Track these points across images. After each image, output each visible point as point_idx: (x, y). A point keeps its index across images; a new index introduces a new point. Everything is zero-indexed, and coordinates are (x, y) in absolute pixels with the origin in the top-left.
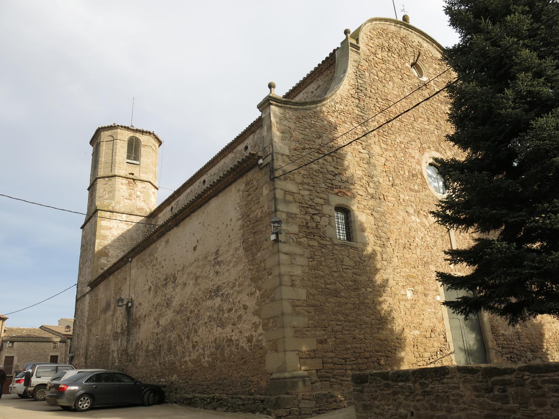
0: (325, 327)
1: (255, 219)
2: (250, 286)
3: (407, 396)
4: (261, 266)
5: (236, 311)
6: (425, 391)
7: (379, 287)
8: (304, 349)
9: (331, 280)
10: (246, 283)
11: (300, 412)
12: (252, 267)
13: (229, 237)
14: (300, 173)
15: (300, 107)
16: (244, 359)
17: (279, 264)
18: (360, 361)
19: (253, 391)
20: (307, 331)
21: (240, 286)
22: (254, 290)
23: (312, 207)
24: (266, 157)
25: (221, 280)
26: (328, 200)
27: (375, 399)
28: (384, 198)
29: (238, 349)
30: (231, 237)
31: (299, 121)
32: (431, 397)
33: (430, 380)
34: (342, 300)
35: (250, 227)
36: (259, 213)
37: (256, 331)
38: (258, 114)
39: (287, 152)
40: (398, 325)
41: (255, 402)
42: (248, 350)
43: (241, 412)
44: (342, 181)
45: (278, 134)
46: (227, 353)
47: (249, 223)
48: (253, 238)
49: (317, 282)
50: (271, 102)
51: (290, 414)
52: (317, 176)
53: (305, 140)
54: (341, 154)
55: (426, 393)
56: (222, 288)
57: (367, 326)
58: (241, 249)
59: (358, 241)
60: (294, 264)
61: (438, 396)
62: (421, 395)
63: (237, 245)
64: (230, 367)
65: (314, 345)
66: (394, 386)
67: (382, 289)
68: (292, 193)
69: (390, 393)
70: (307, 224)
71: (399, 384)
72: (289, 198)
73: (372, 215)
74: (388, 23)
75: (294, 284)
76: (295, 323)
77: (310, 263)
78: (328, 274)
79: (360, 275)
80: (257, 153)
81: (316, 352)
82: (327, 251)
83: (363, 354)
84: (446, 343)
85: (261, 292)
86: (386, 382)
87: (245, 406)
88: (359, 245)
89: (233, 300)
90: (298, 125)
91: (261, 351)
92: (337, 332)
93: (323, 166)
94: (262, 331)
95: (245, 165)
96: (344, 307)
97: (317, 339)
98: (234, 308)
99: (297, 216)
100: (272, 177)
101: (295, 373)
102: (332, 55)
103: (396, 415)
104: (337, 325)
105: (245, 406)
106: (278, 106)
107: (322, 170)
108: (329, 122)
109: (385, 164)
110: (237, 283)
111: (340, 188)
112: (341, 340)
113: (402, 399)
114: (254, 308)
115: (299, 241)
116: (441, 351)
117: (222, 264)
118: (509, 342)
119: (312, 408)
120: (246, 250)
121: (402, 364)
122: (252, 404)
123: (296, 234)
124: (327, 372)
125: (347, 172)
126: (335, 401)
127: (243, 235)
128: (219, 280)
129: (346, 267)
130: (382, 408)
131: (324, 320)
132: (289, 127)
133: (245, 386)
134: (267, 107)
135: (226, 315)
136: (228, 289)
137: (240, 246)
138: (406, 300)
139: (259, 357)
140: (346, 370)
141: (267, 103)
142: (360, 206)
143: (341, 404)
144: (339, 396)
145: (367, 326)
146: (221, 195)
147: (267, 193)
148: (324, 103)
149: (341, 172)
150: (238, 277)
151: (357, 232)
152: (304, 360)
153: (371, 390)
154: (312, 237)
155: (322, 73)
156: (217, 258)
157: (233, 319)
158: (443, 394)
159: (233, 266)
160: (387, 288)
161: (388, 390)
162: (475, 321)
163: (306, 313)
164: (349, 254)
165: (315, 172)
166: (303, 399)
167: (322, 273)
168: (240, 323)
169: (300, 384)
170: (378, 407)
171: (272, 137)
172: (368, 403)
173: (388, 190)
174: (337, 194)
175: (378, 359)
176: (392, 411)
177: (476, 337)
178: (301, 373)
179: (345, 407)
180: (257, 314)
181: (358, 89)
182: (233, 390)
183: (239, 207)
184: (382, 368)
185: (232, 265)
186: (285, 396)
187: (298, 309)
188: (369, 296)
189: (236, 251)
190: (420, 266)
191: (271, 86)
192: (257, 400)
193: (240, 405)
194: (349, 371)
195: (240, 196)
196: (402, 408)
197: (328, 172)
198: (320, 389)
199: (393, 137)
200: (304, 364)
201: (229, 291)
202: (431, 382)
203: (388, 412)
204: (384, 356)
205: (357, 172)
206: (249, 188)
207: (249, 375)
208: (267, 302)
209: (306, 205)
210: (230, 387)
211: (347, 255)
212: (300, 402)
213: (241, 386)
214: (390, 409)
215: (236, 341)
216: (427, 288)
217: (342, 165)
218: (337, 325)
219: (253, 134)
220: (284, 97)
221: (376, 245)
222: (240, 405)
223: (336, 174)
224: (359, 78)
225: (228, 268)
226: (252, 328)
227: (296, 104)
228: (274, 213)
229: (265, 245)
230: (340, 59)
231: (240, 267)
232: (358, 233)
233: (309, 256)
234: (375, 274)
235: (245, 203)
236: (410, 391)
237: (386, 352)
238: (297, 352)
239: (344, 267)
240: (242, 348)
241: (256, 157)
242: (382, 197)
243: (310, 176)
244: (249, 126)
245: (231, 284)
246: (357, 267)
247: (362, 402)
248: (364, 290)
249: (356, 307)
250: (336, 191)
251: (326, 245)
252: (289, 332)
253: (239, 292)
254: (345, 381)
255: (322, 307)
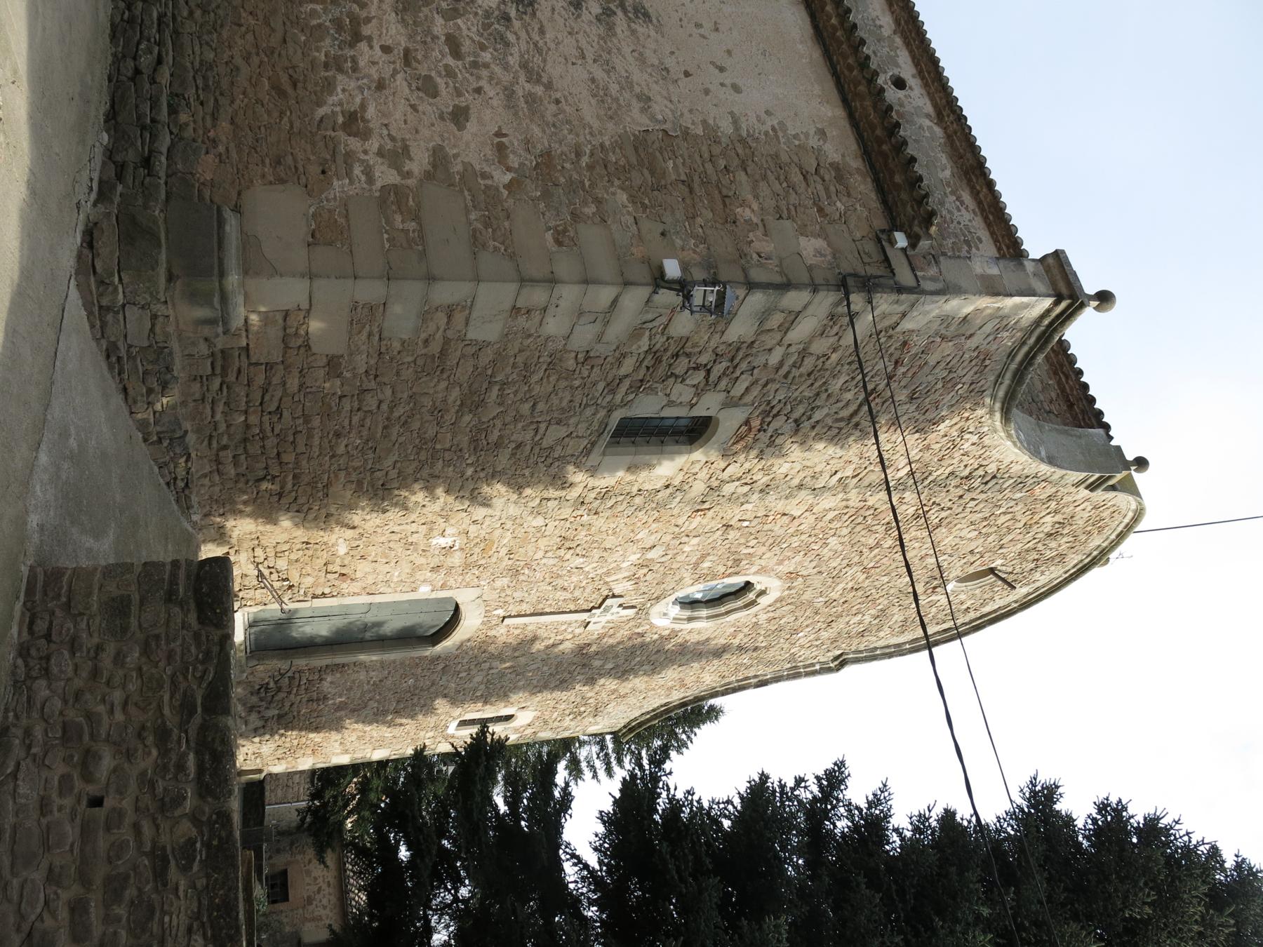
0: (376, 376)
1: (731, 194)
2: (528, 143)
3: (152, 784)
4: (585, 203)
5: (450, 73)
6: (165, 861)
7: (473, 490)
8: (315, 325)
9: (512, 396)
10: (537, 131)
11: (108, 309)
12: (585, 160)
13: (687, 74)
14: (834, 350)
15: (1013, 366)
16: (290, 90)
17: (586, 282)
18: (271, 442)
19: (183, 117)
20: (370, 335)
21: (531, 99)
22: (514, 161)
23: (731, 369)
24: (910, 264)
25: (552, 20)
26: (736, 405)
27: (146, 651)
28: (702, 510)
29: (326, 66)
30: (684, 82)
31: (977, 357)
32: (148, 883)
33: (201, 883)
34: (450, 417)
35: (709, 166)
36: (748, 213)
37: (380, 153)
38: (1036, 246)
39: (907, 325)
40: (366, 519)
41: (143, 128)
42: (321, 112)
43: (110, 58)
44: (777, 433)
45: (968, 309)
46: (313, 12)
47: (722, 163)
48: (674, 177)
49: (514, 366)
50: (1063, 305)
51: (101, 283)
52: (812, 384)
53: (920, 367)
54: (847, 438)
55: (160, 860)
56: (527, 18)
57: (370, 462)
58: (644, 122)
59: (606, 458)
60: (579, 317)
61: (152, 911)
62: (154, 843)
63: (660, 108)
64: (267, 22)
65: (322, 349)
66: (186, 732)
67: (467, 495)
68: (785, 328)
69: (162, 715)
70: (688, 355)
71: (191, 756)
72: (776, 320)
73: (667, 487)
74: (1113, 537)
75: (516, 313)
76: (396, 309)
77: (573, 355)
78: (530, 390)
79: (513, 455)
80: (929, 237)
81: (302, 350)
82: (597, 395)
83: (291, 449)
84: (310, 595)
85: (505, 193)
86: (199, 701)
87: (132, 79)
88: (594, 458)
89: (486, 66)
90: (966, 356)
91: (314, 170)
92: (360, 401)
93: (832, 400)
94: (379, 184)
95: (898, 179)
96: (428, 417)
97: (342, 356)
98: (460, 63)
99: (718, 336)
100: (850, 281)
101: (240, 299)
102: (1095, 419)
103: (92, 736)
104: (381, 402)
105: (132, 79)
106: (1043, 317)
107: (824, 396)
108: (943, 419)
109: (785, 514)
110: (539, 90)
111: (759, 431)
112: (335, 409)
113: (143, 765)
114: (456, 156)
115: (643, 334)
116: (291, 587)
117: (602, 31)
118: (303, 687)
119: (126, 336)
120: (640, 142)
121: (261, 520)
122: (139, 118)
123: (665, 328)
124: (239, 372)
125: (795, 446)
126: (150, 391)
127: (686, 133)
128: (553, 9)
129: (541, 431)
130: (117, 680)
131: (398, 374)
132: (971, 336)
133: (200, 82)
134: (1053, 284)
135: (439, 26)
136: (524, 46)
137: (653, 118)
138: (428, 536)
139: (295, 160)
140: (246, 412)
141: (1064, 291)
142: (698, 466)
143: (141, 405)
144: (165, 400)
145: (370, 462)
146: (817, 54)
147: (804, 253)
148: (998, 416)
149: (800, 434)
150: (558, 95)
151: (631, 457)
152: (281, 322)
153: (175, 640)
154: (646, 363)
155: (1055, 373)
156: (625, 12)
157: (426, 57)
158: (155, 930)
159: (593, 80)
160: (467, 503)
161: (172, 707)
162: (360, 636)
163: (423, 336)
164: (577, 437)
165: (825, 383)
166: (154, 317)
167: (535, 378)
168: (410, 85)
169: (202, 313)
170: (119, 658)
171: (965, 292)
172: (134, 622)
173: (719, 518)
174: (747, 422)
175: (274, 477)
176: (105, 718)
177: (321, 636)
178: (239, 312)
179: (132, 413)
180: (434, 166)
181: (994, 477)
182: (190, 27)
183: (773, 129)
184: (250, 484)
185: (599, 74)
186: (162, 272)
187: (441, 318)
188: (451, 469)
189: (639, 97)
190: (510, 562)
191: (1105, 298)
192: (154, 137)
193: (135, 59)
194: (243, 418)
195: (807, 135)
196: (114, 763)
197: (813, 408)
198: (186, 352)
199: (845, 531)
200: (266, 319)
201: (515, 50)
202: (194, 887)
203: (103, 700)
204: (282, 488)
205: (787, 466)
206: (827, 177)
207: (235, 106)
208: (473, 217)
209: (741, 354)
210: (198, 13)
211: (574, 435)
212: (143, 307)
213: (201, 64)
214: (111, 712)
215: (354, 60)
216: (453, 571)
217: (818, 438)
218: (381, 402)
219: (933, 113)
220: (1063, 346)
221: (586, 490)
222: (135, 59)
223: (798, 426)
224: (1019, 480)
225: (590, 56)
226: (393, 139)
227: (1029, 360)
228: (742, 279)
229: (651, 228)
230: (1083, 442)
231: (590, 112)
232: (628, 459)
233: (592, 354)
234: (509, 485)
235: (784, 158)
236: (167, 799)
237: (294, 494)
238: (305, 306)
239: (543, 426)
240: (329, 86)
241: (916, 229)
242: (706, 506)
243: (819, 371)
244: (961, 109)
245: (537, 60)
246: (536, 450)
247: (137, 597)
248: (469, 461)
249: (426, 443)
250: (756, 423)
251: (613, 392)
252: (369, 291)
253: (509, 94)
254: (212, 409)
255: (438, 373)
